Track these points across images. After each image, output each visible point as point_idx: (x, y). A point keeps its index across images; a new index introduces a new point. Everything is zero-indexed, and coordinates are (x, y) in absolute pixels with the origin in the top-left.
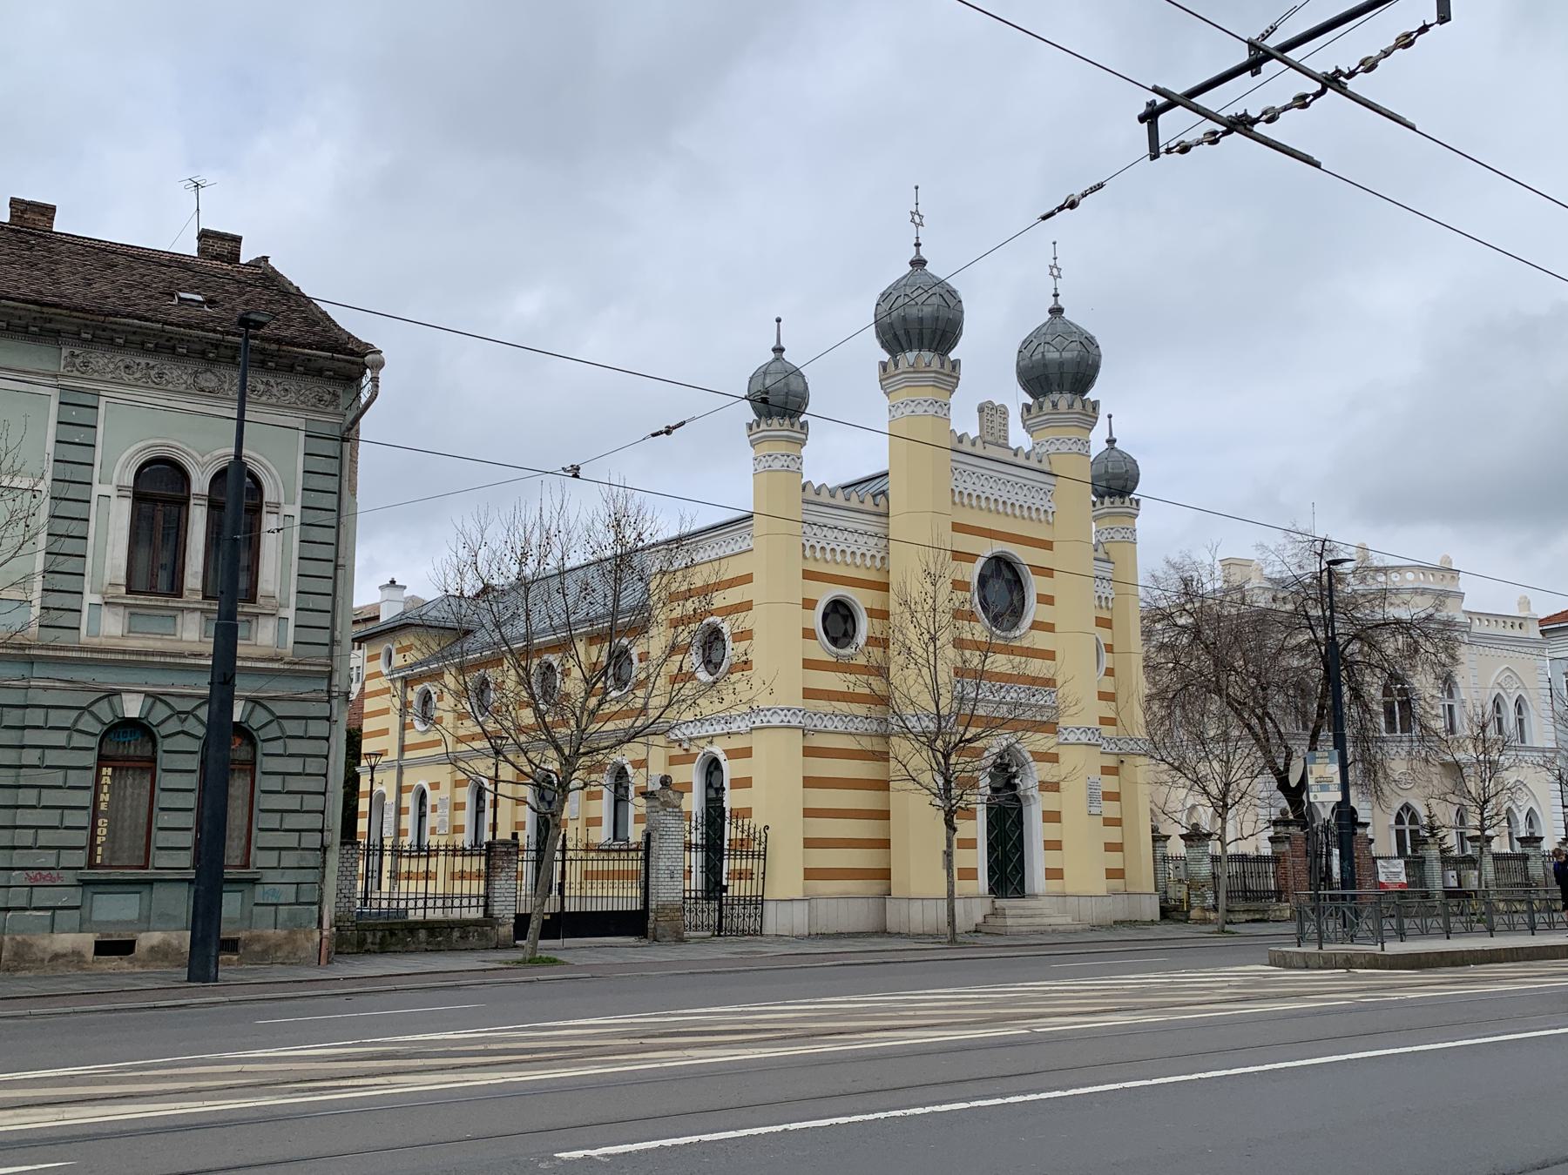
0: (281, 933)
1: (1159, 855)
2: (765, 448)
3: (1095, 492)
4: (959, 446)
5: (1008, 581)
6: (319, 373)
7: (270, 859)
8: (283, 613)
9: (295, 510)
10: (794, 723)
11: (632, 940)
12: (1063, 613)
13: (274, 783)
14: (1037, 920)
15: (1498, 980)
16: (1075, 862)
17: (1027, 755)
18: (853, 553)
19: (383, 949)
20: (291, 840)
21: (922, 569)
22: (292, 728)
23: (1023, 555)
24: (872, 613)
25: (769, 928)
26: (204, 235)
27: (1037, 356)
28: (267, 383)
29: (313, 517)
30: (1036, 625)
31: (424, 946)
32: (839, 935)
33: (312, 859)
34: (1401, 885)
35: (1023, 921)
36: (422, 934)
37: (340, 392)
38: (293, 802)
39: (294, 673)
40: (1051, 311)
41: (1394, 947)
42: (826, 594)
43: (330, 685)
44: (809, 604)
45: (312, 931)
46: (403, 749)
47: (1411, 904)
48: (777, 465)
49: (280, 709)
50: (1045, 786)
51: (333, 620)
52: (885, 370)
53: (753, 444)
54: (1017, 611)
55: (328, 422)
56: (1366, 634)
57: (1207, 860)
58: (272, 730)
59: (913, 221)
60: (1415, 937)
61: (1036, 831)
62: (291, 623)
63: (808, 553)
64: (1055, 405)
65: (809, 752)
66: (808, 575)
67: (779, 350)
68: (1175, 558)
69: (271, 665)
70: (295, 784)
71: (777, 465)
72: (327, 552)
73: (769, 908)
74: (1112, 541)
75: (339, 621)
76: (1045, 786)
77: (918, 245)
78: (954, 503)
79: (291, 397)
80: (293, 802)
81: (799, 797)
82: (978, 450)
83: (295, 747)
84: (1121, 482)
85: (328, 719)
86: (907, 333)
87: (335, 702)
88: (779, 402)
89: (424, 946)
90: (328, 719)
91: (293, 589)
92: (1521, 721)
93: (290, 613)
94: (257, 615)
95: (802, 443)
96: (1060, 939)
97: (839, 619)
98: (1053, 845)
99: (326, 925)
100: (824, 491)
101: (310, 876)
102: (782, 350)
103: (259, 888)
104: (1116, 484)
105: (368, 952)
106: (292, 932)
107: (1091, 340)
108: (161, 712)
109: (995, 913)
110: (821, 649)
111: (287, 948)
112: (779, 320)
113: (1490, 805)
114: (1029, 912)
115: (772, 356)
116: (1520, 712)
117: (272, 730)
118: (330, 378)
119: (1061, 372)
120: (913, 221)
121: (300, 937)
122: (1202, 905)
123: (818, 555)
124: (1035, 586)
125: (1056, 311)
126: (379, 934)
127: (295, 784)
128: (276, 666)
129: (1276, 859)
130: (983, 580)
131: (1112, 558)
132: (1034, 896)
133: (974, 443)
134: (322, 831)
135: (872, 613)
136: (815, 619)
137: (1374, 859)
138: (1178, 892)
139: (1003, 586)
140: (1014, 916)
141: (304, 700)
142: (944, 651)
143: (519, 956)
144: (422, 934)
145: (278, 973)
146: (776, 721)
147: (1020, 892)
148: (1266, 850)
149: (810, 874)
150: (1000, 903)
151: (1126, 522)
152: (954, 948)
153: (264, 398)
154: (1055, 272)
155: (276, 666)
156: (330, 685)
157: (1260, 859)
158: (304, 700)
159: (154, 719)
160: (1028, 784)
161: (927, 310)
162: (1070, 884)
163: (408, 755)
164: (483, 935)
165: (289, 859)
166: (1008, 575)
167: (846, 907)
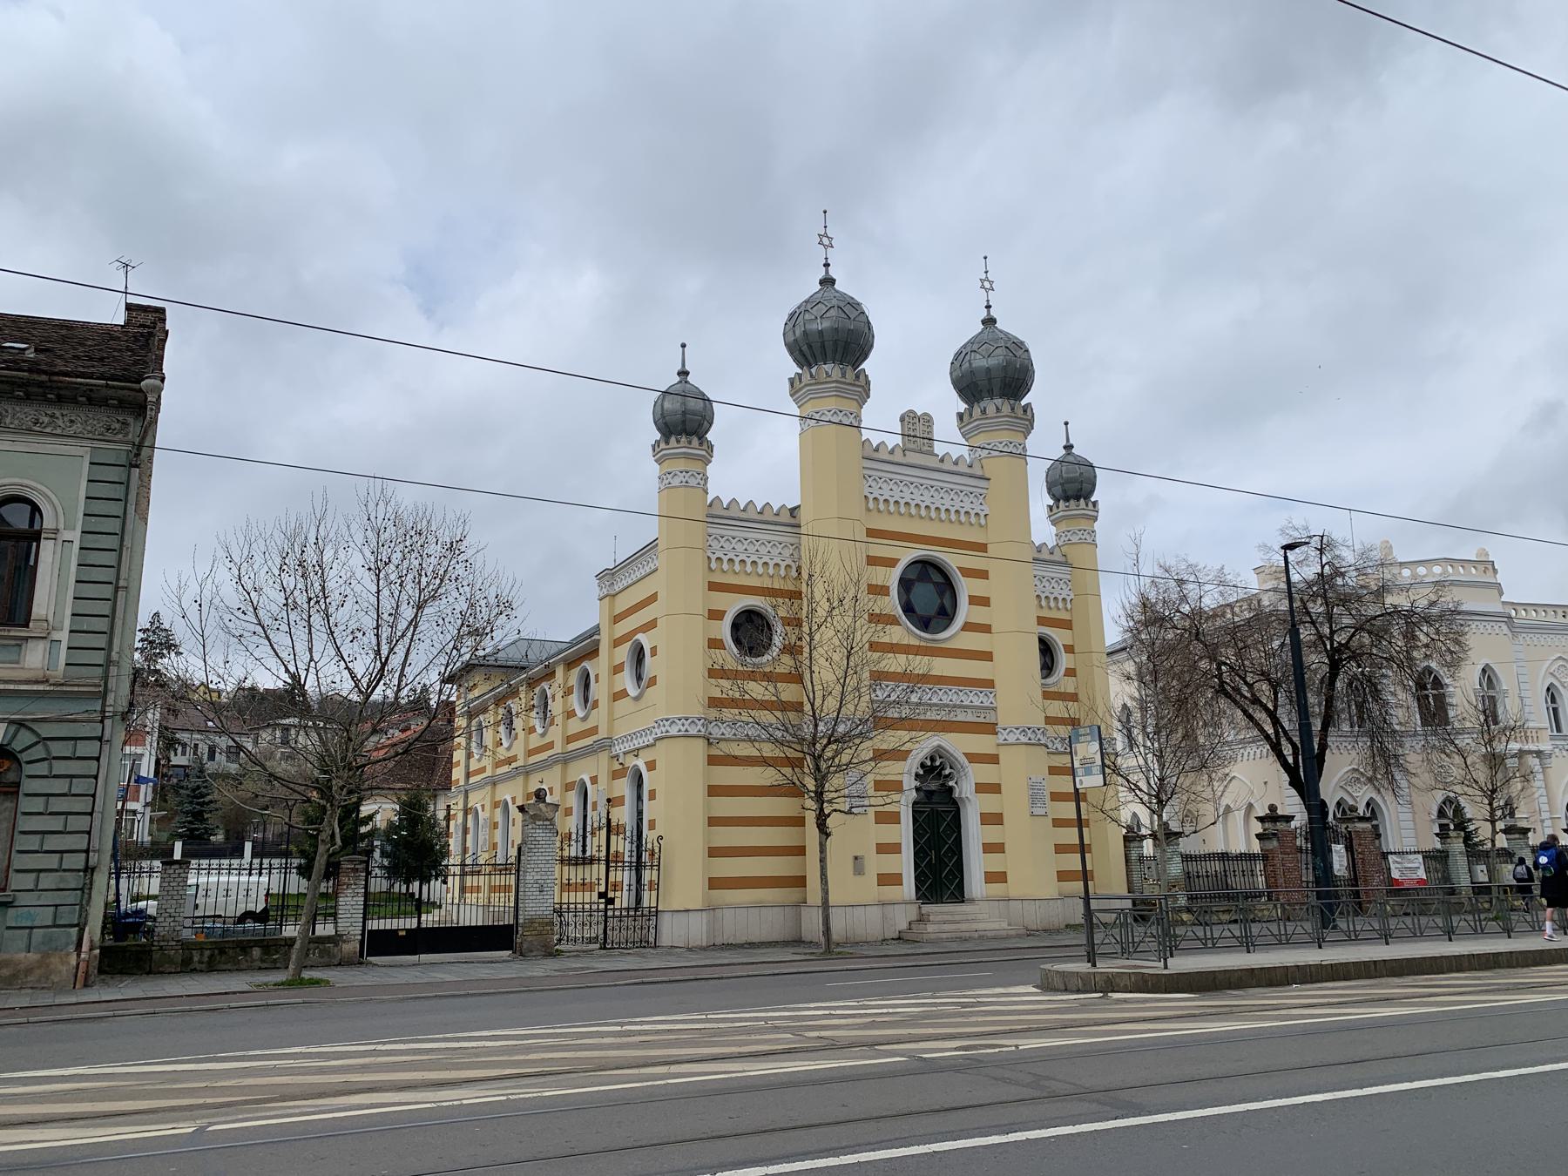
0: (33, 957)
1: (1134, 855)
2: (670, 466)
3: (1053, 496)
4: (872, 454)
5: (936, 584)
6: (103, 403)
7: (28, 881)
8: (56, 636)
9: (75, 535)
10: (693, 731)
11: (506, 953)
12: (999, 612)
13: (37, 805)
14: (964, 927)
15: (1387, 1000)
16: (1018, 865)
17: (963, 759)
18: (742, 561)
19: (211, 968)
20: (52, 861)
21: (845, 577)
22: (57, 749)
23: (952, 560)
24: (787, 622)
25: (666, 939)
26: (129, 307)
27: (966, 365)
28: (52, 416)
29: (92, 541)
30: (968, 627)
31: (258, 964)
32: (752, 945)
33: (73, 881)
34: (1421, 881)
35: (946, 927)
36: (256, 952)
37: (130, 420)
38: (56, 824)
39: (60, 692)
40: (983, 322)
41: (1182, 964)
42: (734, 604)
43: (104, 705)
44: (715, 615)
45: (68, 954)
46: (468, 775)
47: (1436, 900)
48: (676, 482)
49: (46, 730)
50: (981, 788)
51: (110, 642)
52: (792, 385)
53: (1054, 523)
54: (946, 615)
55: (117, 450)
56: (1375, 628)
57: (1179, 859)
58: (38, 752)
59: (983, 287)
60: (1465, 936)
61: (974, 834)
62: (64, 646)
63: (714, 565)
64: (984, 412)
65: (713, 760)
66: (714, 587)
67: (683, 373)
68: (1171, 562)
69: (35, 687)
70: (58, 805)
71: (676, 482)
72: (107, 574)
73: (665, 920)
74: (1069, 543)
75: (116, 642)
76: (981, 788)
77: (827, 265)
78: (869, 510)
79: (77, 427)
80: (56, 824)
81: (697, 805)
82: (898, 457)
83: (60, 768)
84: (1077, 486)
85: (100, 739)
86: (810, 347)
87: (108, 722)
88: (685, 422)
89: (258, 964)
90: (100, 739)
91: (68, 612)
92: (1555, 710)
93: (63, 636)
94: (26, 639)
95: (1095, 519)
96: (995, 945)
97: (751, 630)
98: (991, 848)
99: (85, 947)
100: (1044, 550)
101: (72, 897)
102: (687, 373)
103: (11, 911)
104: (1073, 486)
105: (194, 971)
106: (46, 955)
107: (1020, 345)
108: (25, 738)
109: (922, 919)
110: (730, 656)
111: (38, 972)
112: (684, 346)
113: (1498, 795)
114: (957, 918)
115: (678, 379)
116: (1553, 700)
117: (38, 752)
118: (113, 406)
119: (995, 379)
120: (983, 287)
121: (55, 960)
122: (1175, 912)
123: (1061, 605)
124: (966, 588)
125: (989, 322)
126: (207, 953)
127: (58, 805)
128: (41, 687)
129: (1265, 857)
130: (905, 584)
131: (1069, 563)
132: (972, 901)
133: (892, 452)
134: (87, 851)
135: (787, 622)
136: (724, 630)
137: (1385, 855)
138: (1151, 890)
139: (930, 594)
140: (939, 923)
141: (74, 721)
142: (841, 649)
143: (281, 976)
144: (256, 952)
145: (540, 969)
146: (674, 731)
147: (958, 895)
148: (1256, 847)
149: (715, 883)
150: (927, 908)
151: (1084, 524)
152: (903, 957)
153: (48, 430)
154: (987, 285)
155: (41, 687)
156: (104, 705)
157: (1242, 857)
158: (74, 721)
159: (17, 746)
160: (964, 789)
161: (826, 324)
162: (1013, 888)
163: (472, 780)
164: (327, 953)
165: (47, 881)
166: (938, 578)
167: (755, 916)
